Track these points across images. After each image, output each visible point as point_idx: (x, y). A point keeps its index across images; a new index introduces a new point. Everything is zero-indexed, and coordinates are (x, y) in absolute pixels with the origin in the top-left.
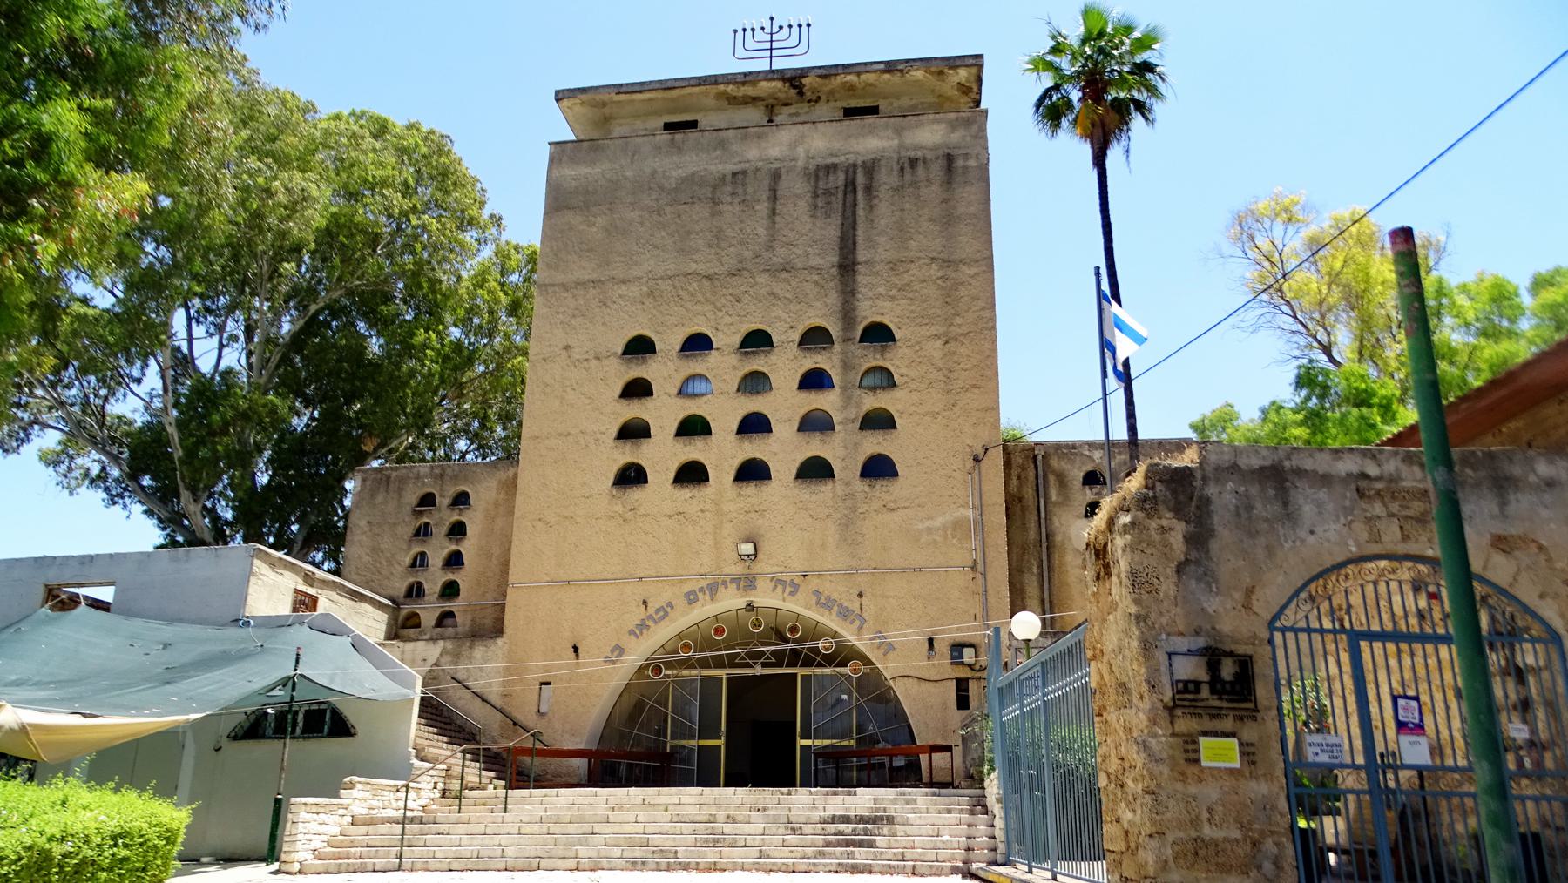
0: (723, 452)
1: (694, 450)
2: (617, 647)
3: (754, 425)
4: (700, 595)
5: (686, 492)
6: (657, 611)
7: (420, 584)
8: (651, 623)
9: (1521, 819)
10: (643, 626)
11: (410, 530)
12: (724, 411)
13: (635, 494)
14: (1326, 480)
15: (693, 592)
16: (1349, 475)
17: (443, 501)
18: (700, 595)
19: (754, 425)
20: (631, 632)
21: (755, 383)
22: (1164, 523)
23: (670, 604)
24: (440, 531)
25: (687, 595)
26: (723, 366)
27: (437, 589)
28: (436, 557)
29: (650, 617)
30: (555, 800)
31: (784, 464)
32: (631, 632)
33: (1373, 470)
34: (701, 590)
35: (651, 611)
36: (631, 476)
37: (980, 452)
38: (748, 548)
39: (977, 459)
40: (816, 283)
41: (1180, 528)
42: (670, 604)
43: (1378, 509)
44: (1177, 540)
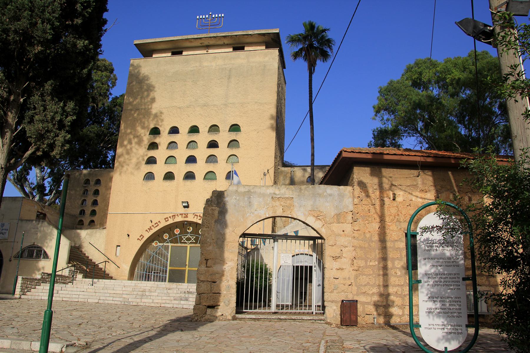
0: (180, 169)
1: (191, 168)
2: (142, 235)
3: (191, 160)
4: (169, 219)
5: (168, 183)
6: (155, 224)
7: (84, 211)
8: (152, 228)
9: (120, 303)
10: (150, 229)
11: (82, 192)
12: (182, 153)
13: (151, 183)
14: (263, 195)
15: (167, 218)
16: (270, 193)
17: (92, 183)
18: (169, 219)
19: (191, 160)
20: (146, 230)
21: (192, 144)
22: (213, 208)
23: (159, 222)
24: (91, 193)
25: (165, 219)
26: (182, 139)
27: (89, 212)
28: (89, 201)
29: (153, 226)
30: (181, 287)
31: (179, 175)
32: (146, 230)
33: (277, 192)
34: (170, 217)
35: (153, 224)
36: (149, 176)
37: (266, 172)
38: (186, 204)
39: (265, 175)
40: (215, 110)
41: (217, 209)
42: (159, 222)
43: (277, 203)
44: (216, 213)
